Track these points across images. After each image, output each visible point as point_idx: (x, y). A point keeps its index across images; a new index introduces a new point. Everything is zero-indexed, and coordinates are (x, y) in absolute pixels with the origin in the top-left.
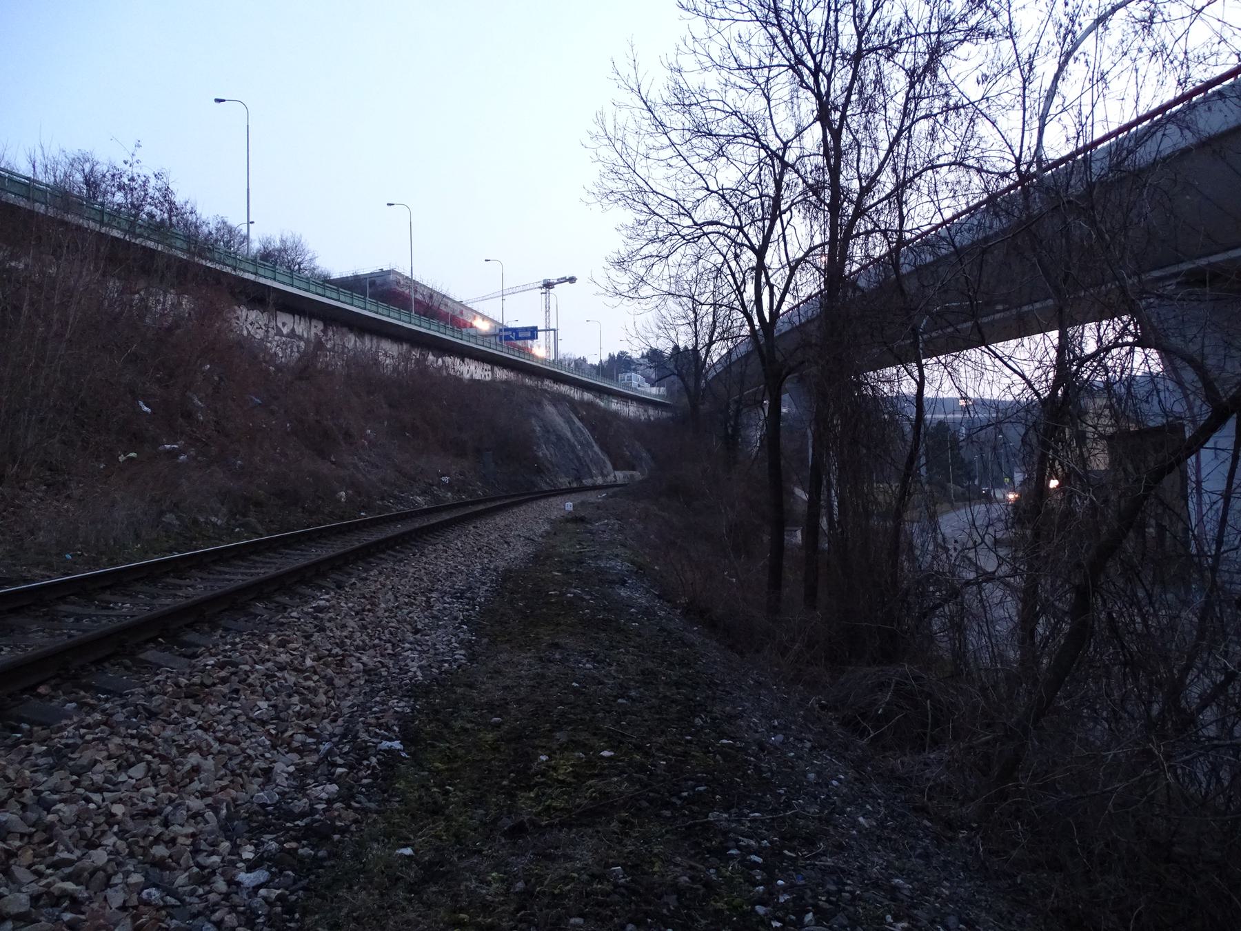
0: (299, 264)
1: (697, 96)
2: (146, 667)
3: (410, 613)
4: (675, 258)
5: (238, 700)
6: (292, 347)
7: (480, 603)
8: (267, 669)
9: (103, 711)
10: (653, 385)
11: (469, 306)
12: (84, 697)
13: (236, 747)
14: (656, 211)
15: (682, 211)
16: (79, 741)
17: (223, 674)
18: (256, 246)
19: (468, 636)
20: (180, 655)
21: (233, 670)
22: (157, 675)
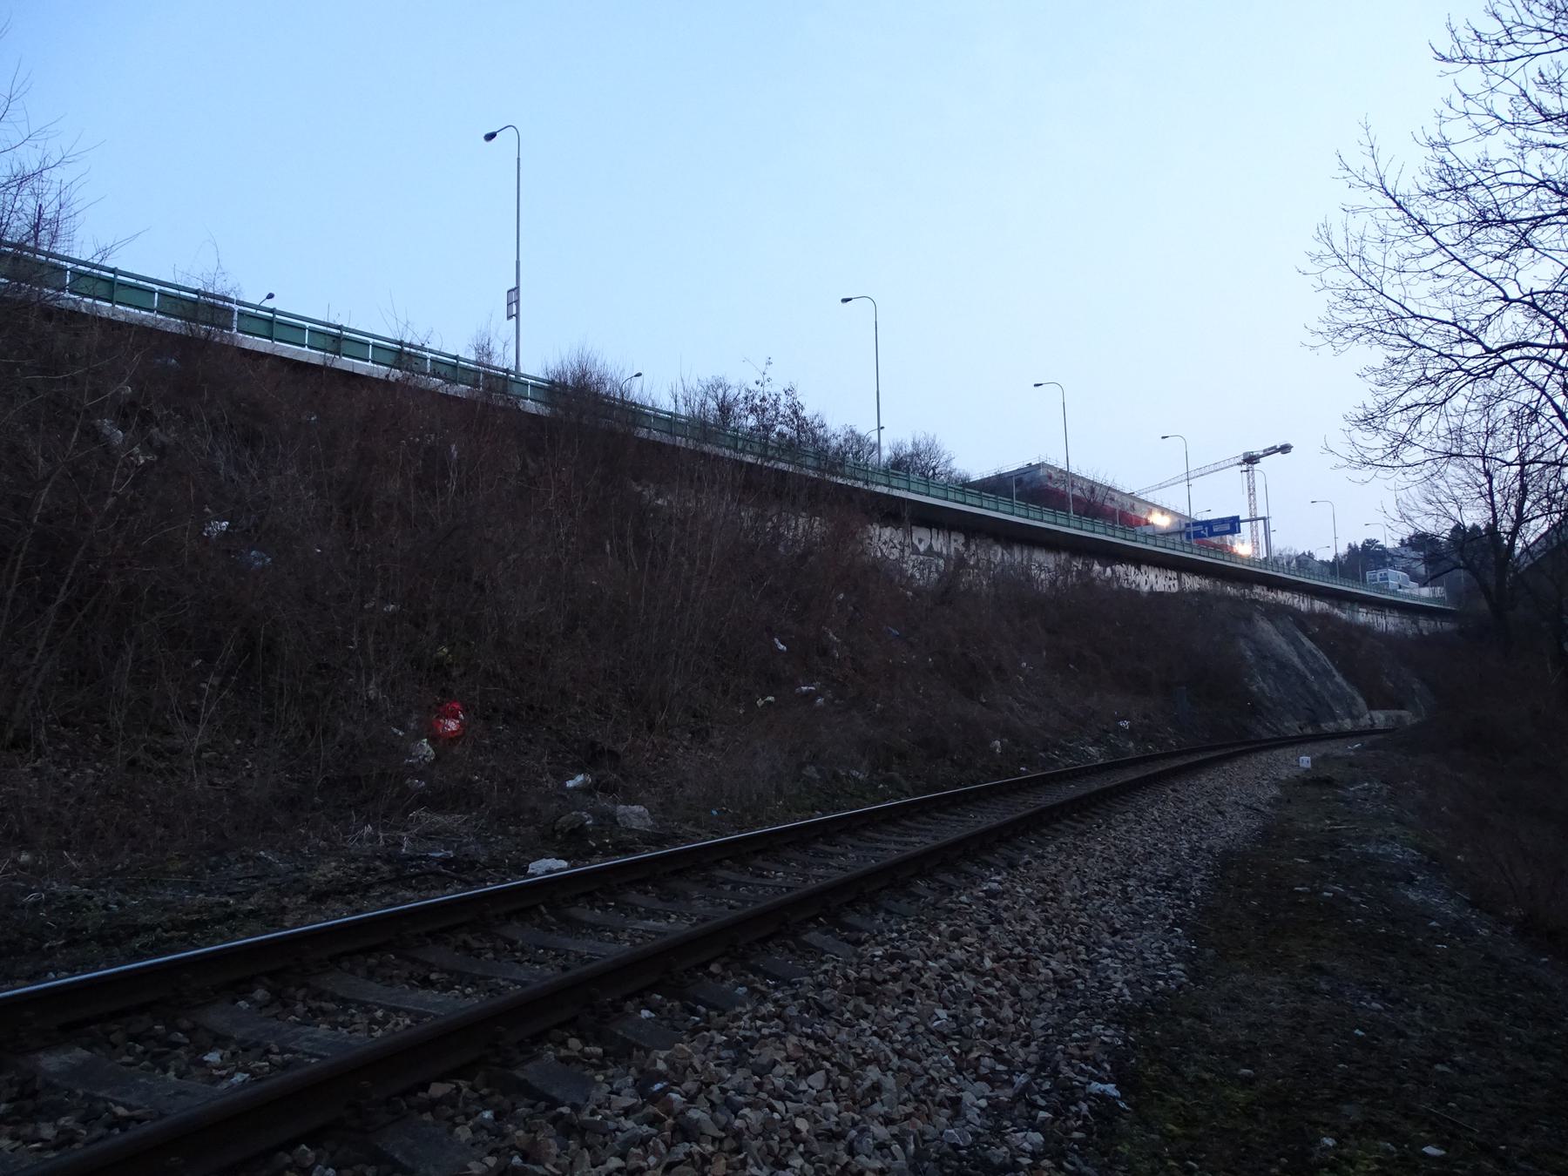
0: (934, 469)
1: (1477, 173)
2: (811, 952)
3: (1103, 905)
4: (1459, 402)
5: (913, 1004)
6: (930, 568)
7: (1196, 899)
8: (942, 968)
9: (776, 1001)
10: (1425, 585)
11: (1143, 497)
12: (754, 982)
13: (918, 1066)
14: (1421, 342)
15: (1464, 335)
16: (757, 1036)
17: (893, 969)
18: (886, 453)
19: (1185, 944)
20: (842, 940)
21: (904, 965)
22: (823, 962)
